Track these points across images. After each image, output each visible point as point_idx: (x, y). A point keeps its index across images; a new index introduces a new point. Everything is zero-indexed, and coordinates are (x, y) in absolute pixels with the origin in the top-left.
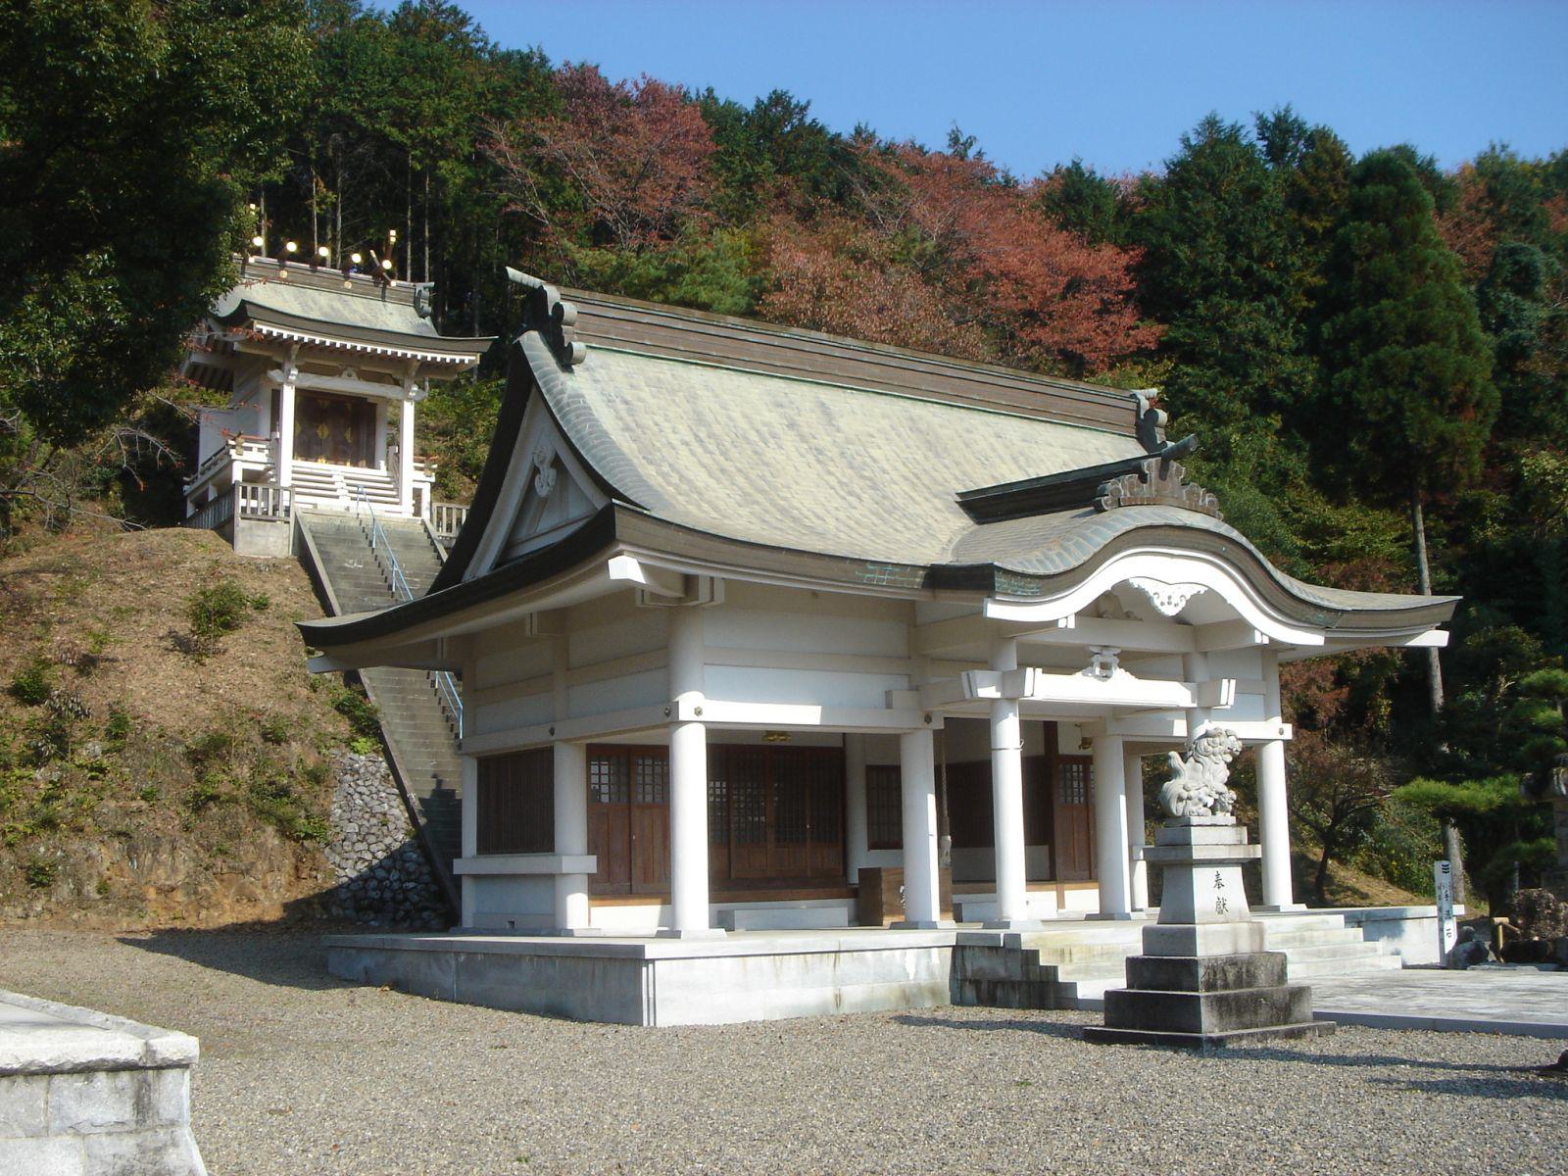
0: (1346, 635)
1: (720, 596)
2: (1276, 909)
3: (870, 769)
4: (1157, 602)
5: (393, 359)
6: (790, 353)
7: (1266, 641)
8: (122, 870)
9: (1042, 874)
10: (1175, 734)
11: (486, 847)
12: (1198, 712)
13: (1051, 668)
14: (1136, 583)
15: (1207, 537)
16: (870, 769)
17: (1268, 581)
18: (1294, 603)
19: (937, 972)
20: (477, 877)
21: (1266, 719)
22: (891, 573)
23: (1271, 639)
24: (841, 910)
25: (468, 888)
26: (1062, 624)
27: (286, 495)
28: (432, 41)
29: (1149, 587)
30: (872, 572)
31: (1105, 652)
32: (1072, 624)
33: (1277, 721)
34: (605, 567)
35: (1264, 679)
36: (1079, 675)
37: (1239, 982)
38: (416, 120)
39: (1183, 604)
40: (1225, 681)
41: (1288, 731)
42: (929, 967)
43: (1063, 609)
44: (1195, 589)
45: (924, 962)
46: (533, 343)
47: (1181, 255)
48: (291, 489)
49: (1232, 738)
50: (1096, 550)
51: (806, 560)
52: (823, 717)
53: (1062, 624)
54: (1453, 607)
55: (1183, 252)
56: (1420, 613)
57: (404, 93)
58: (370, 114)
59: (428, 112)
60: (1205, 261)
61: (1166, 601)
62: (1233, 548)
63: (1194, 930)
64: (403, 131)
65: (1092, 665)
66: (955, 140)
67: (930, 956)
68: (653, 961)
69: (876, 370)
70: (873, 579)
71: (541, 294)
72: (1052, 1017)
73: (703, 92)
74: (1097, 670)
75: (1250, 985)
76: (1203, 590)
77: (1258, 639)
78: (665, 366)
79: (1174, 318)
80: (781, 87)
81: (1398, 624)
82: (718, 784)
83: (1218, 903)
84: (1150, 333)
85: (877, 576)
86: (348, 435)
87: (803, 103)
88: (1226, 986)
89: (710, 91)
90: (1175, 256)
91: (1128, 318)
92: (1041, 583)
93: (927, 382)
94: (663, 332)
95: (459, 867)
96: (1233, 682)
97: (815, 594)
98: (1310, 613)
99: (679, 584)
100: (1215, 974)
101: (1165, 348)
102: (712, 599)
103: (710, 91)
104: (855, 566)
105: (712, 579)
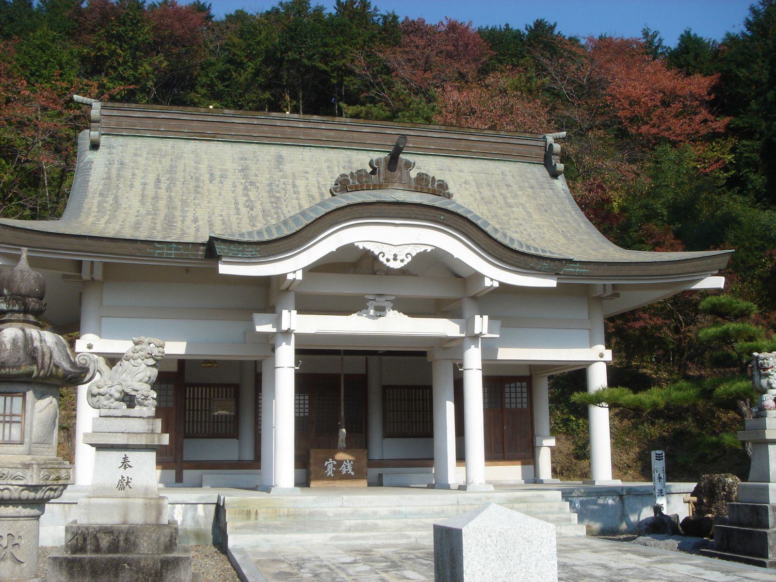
1: (98, 274)
2: (541, 482)
3: (385, 389)
4: (382, 259)
6: (266, 128)
7: (496, 285)
8: (64, 447)
9: (496, 452)
10: (498, 358)
12: (467, 341)
13: (301, 310)
14: (356, 244)
15: (423, 209)
16: (385, 389)
17: (488, 240)
18: (514, 255)
19: (202, 521)
21: (591, 346)
22: (176, 249)
23: (501, 284)
26: (290, 277)
28: (354, 17)
29: (375, 249)
32: (299, 276)
33: (601, 348)
35: (589, 318)
36: (354, 316)
37: (114, 547)
38: (334, 57)
39: (408, 260)
40: (477, 317)
41: (608, 355)
42: (194, 518)
44: (422, 249)
45: (190, 514)
47: (741, 75)
49: (152, 345)
50: (308, 222)
51: (105, 243)
52: (187, 350)
53: (290, 277)
54: (727, 258)
55: (742, 73)
56: (695, 263)
57: (326, 45)
58: (310, 58)
59: (338, 52)
60: (755, 76)
61: (391, 257)
62: (452, 217)
63: (767, 488)
64: (326, 64)
65: (367, 308)
66: (646, 34)
67: (196, 510)
69: (332, 133)
70: (163, 254)
72: (425, 550)
73: (503, 26)
74: (372, 312)
75: (126, 551)
77: (488, 283)
78: (171, 142)
79: (741, 113)
80: (540, 17)
81: (671, 272)
82: (302, 398)
83: (121, 481)
84: (720, 123)
85: (165, 251)
87: (552, 23)
88: (98, 550)
89: (507, 25)
90: (737, 76)
91: (704, 113)
92: (258, 248)
93: (369, 139)
94: (173, 123)
96: (486, 317)
97: (187, 270)
98: (533, 263)
100: (85, 540)
101: (730, 131)
103: (507, 25)
104: (145, 246)
105: (92, 262)
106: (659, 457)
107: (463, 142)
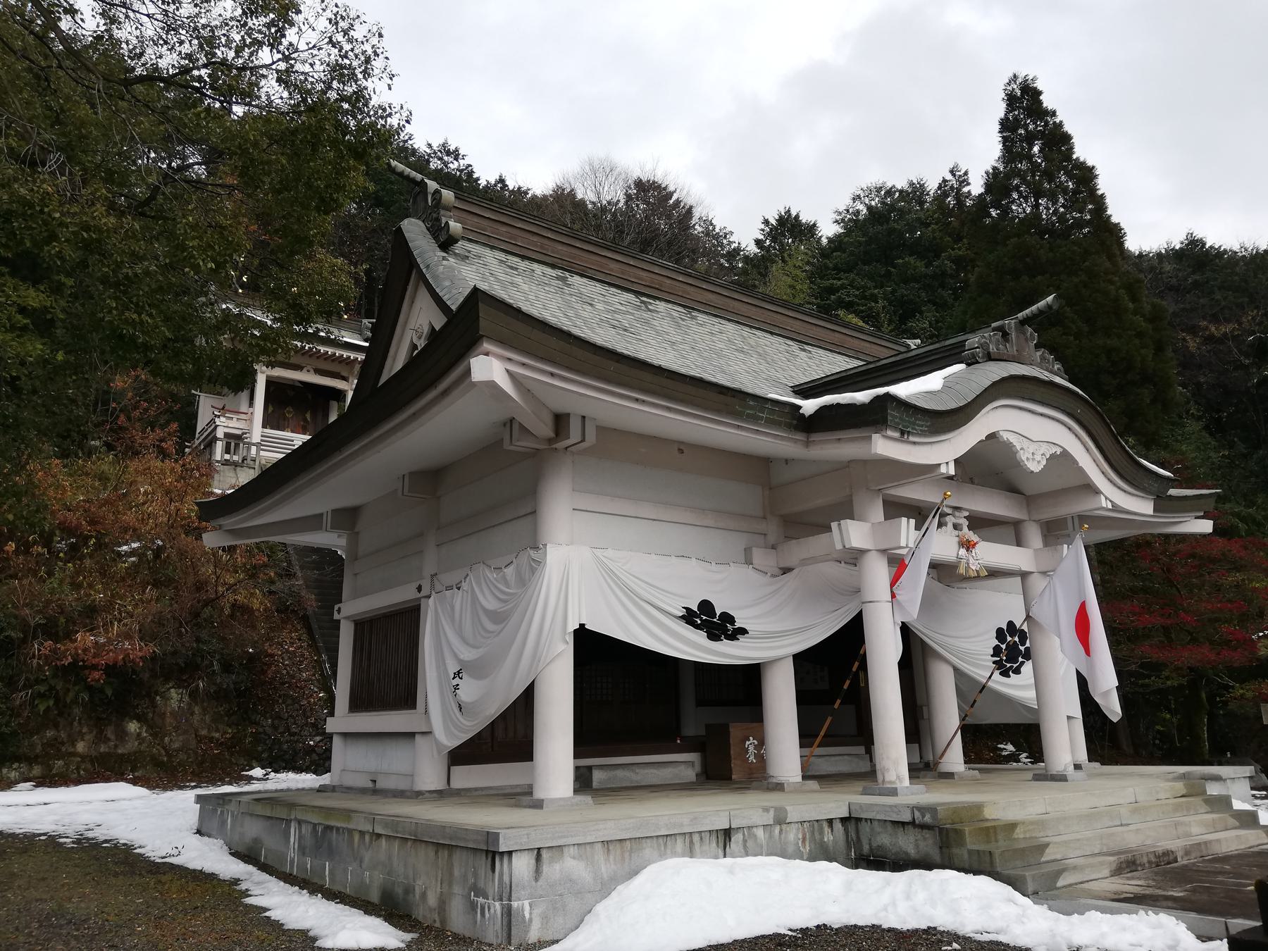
0: (786, 642)
5: (341, 360)
11: (359, 703)
14: (1005, 436)
20: (346, 735)
24: (684, 764)
25: (337, 743)
26: (943, 469)
27: (254, 449)
30: (751, 408)
31: (957, 514)
34: (468, 372)
43: (944, 452)
46: (414, 229)
48: (258, 445)
68: (510, 853)
71: (422, 185)
76: (1059, 451)
86: (308, 416)
95: (332, 725)
99: (549, 420)
102: (583, 440)
107: (837, 335)
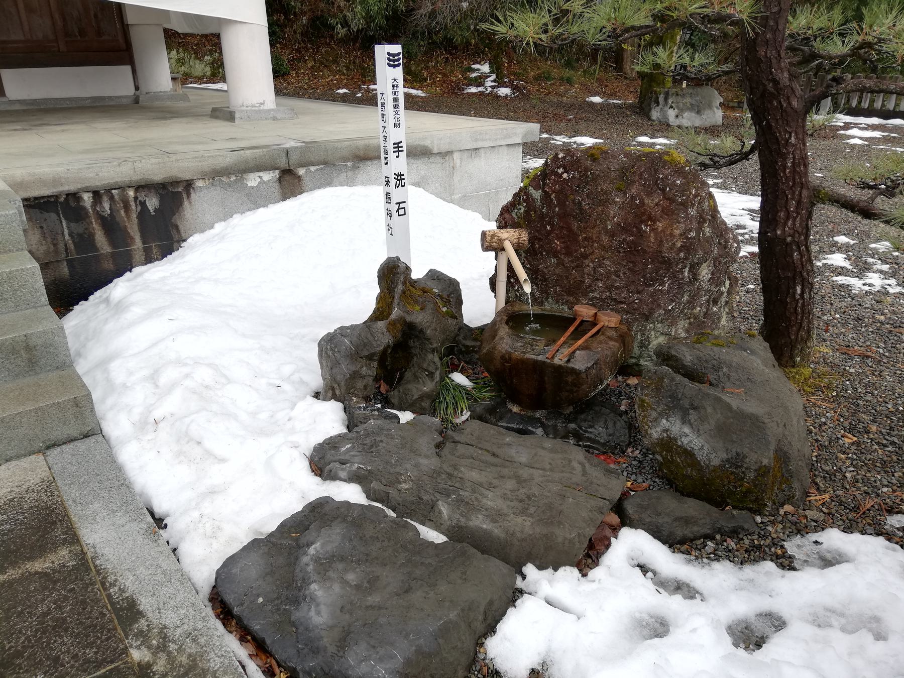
106: (393, 62)
